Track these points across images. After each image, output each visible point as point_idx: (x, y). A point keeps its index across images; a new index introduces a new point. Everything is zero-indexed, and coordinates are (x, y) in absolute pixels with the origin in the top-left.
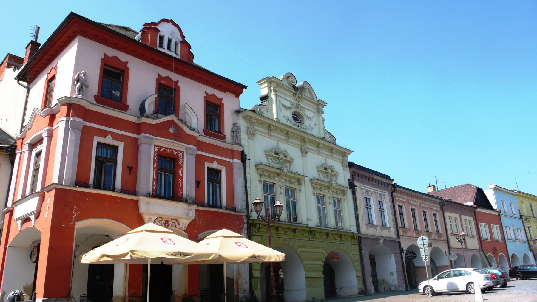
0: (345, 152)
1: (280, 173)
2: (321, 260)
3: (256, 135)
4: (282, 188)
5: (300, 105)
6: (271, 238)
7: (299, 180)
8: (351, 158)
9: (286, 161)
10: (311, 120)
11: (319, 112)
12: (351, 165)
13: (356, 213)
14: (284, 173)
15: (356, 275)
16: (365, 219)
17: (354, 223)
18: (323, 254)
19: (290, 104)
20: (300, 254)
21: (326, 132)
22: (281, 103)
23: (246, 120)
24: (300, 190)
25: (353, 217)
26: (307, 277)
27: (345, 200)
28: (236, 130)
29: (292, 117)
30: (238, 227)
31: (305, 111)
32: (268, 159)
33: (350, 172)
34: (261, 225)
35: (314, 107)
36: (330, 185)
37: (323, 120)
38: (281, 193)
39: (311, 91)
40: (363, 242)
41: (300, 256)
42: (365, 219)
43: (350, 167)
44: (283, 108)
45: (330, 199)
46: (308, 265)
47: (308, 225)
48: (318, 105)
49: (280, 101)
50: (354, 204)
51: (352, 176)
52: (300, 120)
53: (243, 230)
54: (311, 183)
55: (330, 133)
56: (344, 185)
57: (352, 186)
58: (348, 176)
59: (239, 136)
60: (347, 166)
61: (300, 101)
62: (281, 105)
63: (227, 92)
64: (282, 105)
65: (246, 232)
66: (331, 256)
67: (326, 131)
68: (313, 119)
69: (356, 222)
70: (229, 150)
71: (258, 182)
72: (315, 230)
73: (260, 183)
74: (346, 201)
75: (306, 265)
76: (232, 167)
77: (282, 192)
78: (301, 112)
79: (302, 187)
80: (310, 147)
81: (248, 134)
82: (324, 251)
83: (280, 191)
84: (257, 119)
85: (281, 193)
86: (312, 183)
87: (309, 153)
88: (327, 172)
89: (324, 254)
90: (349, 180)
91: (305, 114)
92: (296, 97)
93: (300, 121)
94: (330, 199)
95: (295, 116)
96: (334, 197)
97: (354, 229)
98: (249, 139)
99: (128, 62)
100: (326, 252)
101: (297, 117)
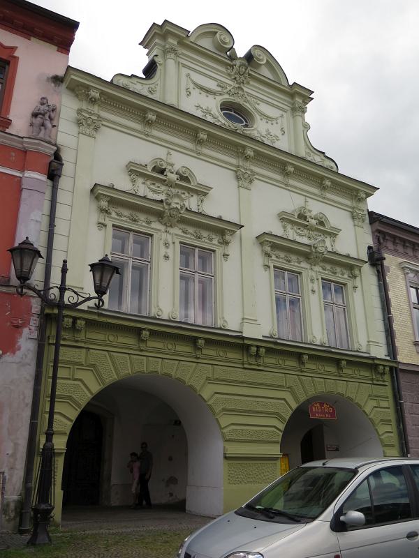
0: (356, 191)
1: (164, 212)
2: (279, 416)
3: (103, 128)
4: (316, 281)
5: (242, 89)
6: (61, 348)
7: (223, 230)
8: (375, 204)
9: (325, 233)
10: (274, 122)
11: (294, 110)
12: (374, 218)
13: (386, 316)
14: (318, 254)
15: (225, 454)
16: (411, 332)
17: (381, 338)
18: (283, 402)
19: (217, 86)
20: (209, 400)
21: (312, 151)
22: (192, 81)
23: (77, 96)
24: (226, 256)
25: (379, 326)
26: (227, 455)
27: (355, 288)
28: (44, 116)
29: (224, 114)
30: (9, 324)
31: (258, 104)
32: (284, 227)
33: (373, 233)
34: (261, 349)
35: (285, 100)
36: (311, 250)
37: (307, 127)
38: (167, 257)
39: (273, 64)
40: (404, 380)
41: (370, 417)
42: (411, 332)
43: (371, 223)
44: (198, 90)
45: (167, 247)
46: (274, 429)
47: (242, 333)
48: (292, 96)
49: (188, 75)
50: (381, 297)
51: (379, 239)
52: (246, 122)
53: (26, 331)
54: (260, 243)
55: (324, 153)
56: (354, 255)
57: (376, 260)
58: (369, 240)
59: (54, 126)
60: (363, 221)
61: (243, 83)
62: (192, 86)
63: (32, 38)
64: (195, 84)
65: (35, 335)
66: (314, 408)
67: (312, 148)
68: (279, 121)
69: (387, 337)
70: (14, 149)
71: (94, 228)
72: (259, 344)
73: (100, 230)
74: (359, 289)
75: (383, 434)
76: (20, 186)
77: (316, 288)
78: (248, 105)
79: (233, 250)
80: (104, 114)
81: (79, 123)
82: (288, 396)
83: (310, 289)
84: (255, 151)
85: (313, 291)
86: (261, 244)
87: (256, 182)
88: (165, 180)
89: (286, 402)
90: (370, 248)
91: (255, 109)
92: (233, 73)
93: (245, 123)
94: (167, 247)
95: (232, 113)
96: (327, 280)
97: (380, 352)
98: (80, 135)
99: (17, 47)
100: (296, 398)
101: (234, 111)
